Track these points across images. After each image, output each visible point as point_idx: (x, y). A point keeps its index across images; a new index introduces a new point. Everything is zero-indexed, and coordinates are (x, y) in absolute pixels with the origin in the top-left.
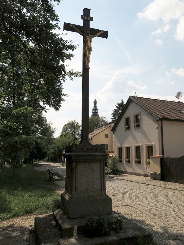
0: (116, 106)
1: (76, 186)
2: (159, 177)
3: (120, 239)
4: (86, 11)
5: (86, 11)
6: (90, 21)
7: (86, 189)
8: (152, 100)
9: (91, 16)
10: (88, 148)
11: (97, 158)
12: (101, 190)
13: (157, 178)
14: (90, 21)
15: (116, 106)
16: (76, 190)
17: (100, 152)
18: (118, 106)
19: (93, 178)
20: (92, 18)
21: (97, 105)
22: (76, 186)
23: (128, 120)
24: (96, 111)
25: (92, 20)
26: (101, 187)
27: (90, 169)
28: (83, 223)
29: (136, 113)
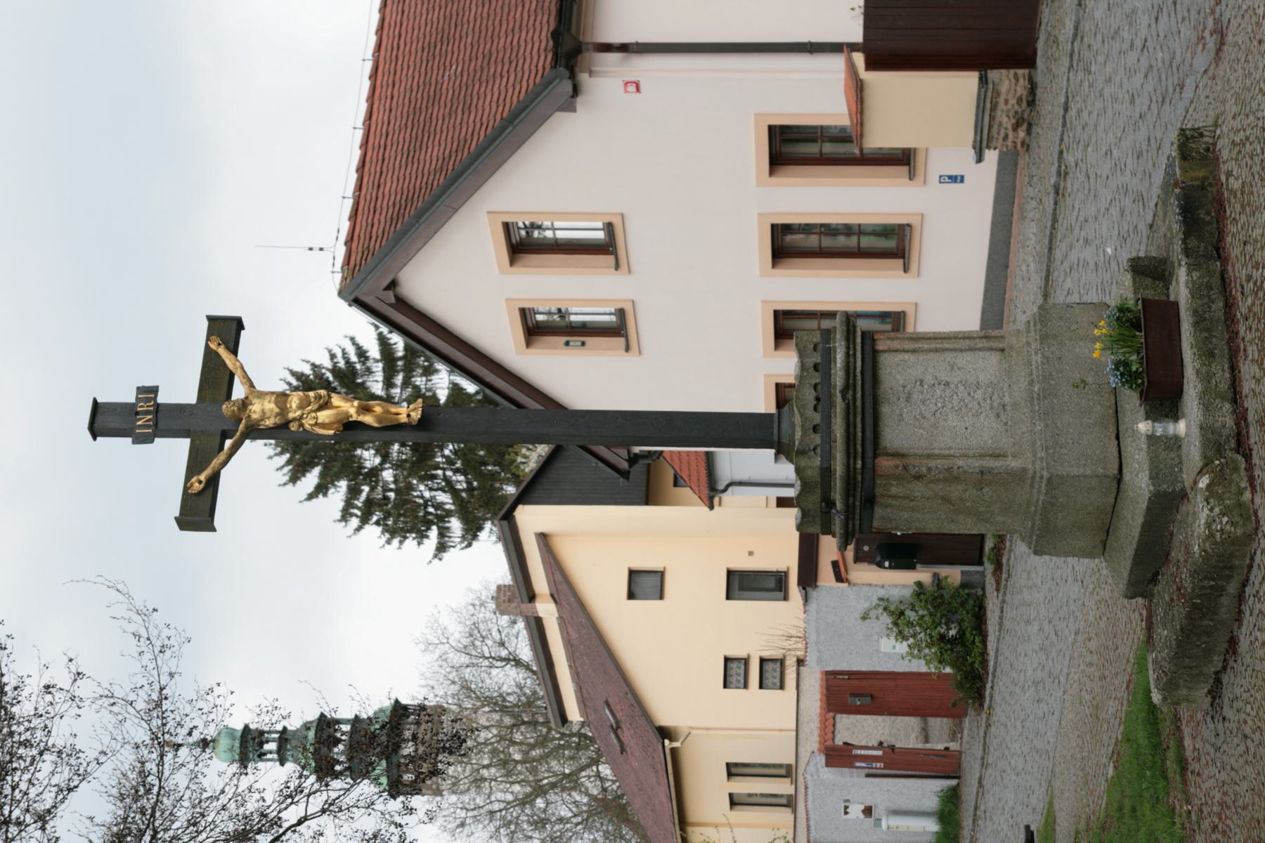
0: (311, 497)
1: (982, 456)
2: (1007, 82)
3: (1187, 256)
6: (160, 400)
7: (998, 416)
8: (379, 116)
9: (130, 398)
11: (859, 363)
12: (1002, 350)
13: (1019, 100)
14: (160, 400)
15: (311, 497)
16: (999, 456)
17: (828, 355)
18: (312, 478)
19: (947, 384)
20: (141, 390)
22: (982, 456)
25: (154, 390)
26: (991, 349)
27: (908, 399)
28: (1131, 400)
29: (494, 248)
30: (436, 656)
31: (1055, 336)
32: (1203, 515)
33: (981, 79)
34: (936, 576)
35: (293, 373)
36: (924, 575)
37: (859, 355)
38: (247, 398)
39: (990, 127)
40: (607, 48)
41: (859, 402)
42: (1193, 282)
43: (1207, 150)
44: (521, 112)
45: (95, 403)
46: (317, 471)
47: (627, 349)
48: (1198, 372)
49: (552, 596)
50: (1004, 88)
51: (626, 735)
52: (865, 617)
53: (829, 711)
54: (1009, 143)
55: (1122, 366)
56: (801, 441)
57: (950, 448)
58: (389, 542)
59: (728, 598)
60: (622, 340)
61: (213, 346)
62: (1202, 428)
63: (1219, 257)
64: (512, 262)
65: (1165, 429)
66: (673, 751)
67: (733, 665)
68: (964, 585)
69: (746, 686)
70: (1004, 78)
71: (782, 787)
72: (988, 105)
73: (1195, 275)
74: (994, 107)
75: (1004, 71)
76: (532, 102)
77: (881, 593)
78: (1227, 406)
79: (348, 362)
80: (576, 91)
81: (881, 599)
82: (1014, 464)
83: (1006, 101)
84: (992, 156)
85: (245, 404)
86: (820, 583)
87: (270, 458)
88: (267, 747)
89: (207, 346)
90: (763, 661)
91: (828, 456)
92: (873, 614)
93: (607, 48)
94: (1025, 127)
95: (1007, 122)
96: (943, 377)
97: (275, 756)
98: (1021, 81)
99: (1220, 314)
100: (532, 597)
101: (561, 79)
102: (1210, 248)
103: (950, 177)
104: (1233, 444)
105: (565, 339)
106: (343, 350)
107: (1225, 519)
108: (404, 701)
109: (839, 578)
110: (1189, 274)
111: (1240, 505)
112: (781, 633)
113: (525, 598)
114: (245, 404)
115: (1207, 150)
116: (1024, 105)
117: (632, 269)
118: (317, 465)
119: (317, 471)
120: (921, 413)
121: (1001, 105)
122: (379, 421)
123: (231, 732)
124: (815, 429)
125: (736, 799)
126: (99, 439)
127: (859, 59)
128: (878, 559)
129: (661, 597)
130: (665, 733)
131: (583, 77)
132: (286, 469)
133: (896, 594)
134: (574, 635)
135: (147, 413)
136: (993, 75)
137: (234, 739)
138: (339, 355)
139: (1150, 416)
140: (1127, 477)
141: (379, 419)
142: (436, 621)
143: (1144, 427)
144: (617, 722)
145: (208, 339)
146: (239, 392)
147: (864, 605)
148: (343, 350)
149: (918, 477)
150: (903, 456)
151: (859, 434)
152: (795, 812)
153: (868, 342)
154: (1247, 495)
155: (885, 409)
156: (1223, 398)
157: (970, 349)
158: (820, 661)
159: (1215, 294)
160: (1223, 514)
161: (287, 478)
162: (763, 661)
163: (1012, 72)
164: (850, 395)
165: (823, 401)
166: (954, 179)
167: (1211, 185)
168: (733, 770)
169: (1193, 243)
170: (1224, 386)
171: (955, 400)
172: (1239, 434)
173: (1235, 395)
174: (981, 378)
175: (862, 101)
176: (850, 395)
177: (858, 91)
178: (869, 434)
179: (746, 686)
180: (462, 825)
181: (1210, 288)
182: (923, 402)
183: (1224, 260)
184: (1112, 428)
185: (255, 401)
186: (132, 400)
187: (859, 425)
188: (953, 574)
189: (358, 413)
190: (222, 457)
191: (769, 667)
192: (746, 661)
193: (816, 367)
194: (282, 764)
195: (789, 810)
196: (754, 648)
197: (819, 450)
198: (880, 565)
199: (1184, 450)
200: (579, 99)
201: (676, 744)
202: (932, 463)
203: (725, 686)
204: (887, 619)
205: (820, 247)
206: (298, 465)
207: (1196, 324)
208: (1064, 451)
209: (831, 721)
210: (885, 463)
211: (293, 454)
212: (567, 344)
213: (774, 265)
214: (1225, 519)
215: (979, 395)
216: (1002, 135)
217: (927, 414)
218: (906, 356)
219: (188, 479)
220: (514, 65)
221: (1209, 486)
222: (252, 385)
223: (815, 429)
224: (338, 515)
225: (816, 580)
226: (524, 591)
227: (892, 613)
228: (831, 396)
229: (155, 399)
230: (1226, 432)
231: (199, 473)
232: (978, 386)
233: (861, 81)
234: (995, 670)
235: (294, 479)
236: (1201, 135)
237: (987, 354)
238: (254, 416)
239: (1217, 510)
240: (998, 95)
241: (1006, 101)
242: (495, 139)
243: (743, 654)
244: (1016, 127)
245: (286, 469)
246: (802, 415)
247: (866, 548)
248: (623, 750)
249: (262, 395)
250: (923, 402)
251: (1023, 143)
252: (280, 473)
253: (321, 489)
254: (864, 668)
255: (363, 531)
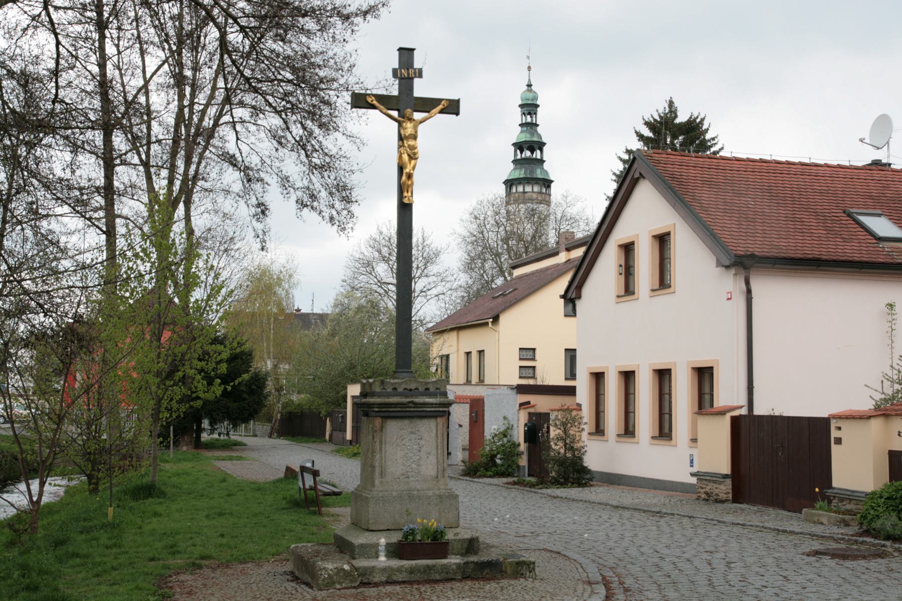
2: (725, 489)
3: (464, 563)
4: (406, 54)
5: (406, 54)
7: (403, 475)
9: (417, 65)
10: (409, 388)
11: (429, 409)
12: (437, 477)
13: (717, 495)
17: (434, 395)
18: (647, 133)
19: (420, 451)
20: (420, 71)
21: (542, 116)
23: (628, 249)
24: (537, 154)
25: (420, 75)
26: (438, 472)
27: (412, 433)
28: (396, 537)
30: (560, 201)
31: (441, 502)
32: (330, 566)
33: (727, 475)
34: (523, 453)
35: (703, 120)
36: (523, 447)
37: (433, 409)
38: (414, 120)
39: (706, 480)
40: (747, 283)
41: (408, 409)
42: (450, 566)
43: (522, 574)
44: (715, 239)
45: (413, 50)
46: (651, 135)
47: (618, 297)
48: (402, 566)
49: (569, 260)
50: (722, 487)
51: (500, 300)
52: (505, 418)
53: (471, 400)
54: (700, 490)
55: (412, 532)
56: (389, 382)
57: (385, 452)
58: (614, 174)
59: (566, 350)
60: (623, 294)
61: (443, 102)
62: (373, 567)
63: (464, 578)
64: (654, 237)
65: (381, 551)
66: (487, 324)
67: (531, 353)
68: (518, 467)
69: (521, 359)
70: (727, 487)
71: (475, 379)
72: (714, 479)
73: (454, 567)
74: (715, 482)
75: (730, 487)
76: (720, 244)
77: (515, 426)
78: (384, 579)
79: (711, 147)
80: (727, 267)
81: (512, 426)
82: (377, 482)
83: (717, 488)
84: (694, 480)
85: (411, 119)
86: (519, 395)
87: (657, 111)
88: (529, 117)
89: (443, 100)
90: (534, 368)
91: (380, 395)
92: (506, 422)
93: (747, 283)
94: (707, 498)
95: (708, 489)
96: (423, 449)
97: (524, 122)
98: (725, 496)
99: (433, 577)
100: (568, 250)
101: (729, 259)
102: (468, 574)
103: (692, 460)
104: (365, 581)
105: (623, 264)
106: (716, 143)
107: (326, 576)
108: (553, 185)
109: (521, 405)
110: (455, 564)
111: (334, 583)
112: (545, 376)
113: (568, 246)
114: (411, 119)
115: (522, 574)
116: (715, 497)
117: (653, 298)
118: (654, 134)
119: (651, 135)
120: (404, 439)
121: (716, 486)
122: (404, 183)
123: (536, 98)
124: (395, 389)
125: (482, 354)
126: (398, 52)
127: (744, 411)
128: (529, 424)
129: (566, 316)
130: (496, 319)
131: (733, 271)
132: (652, 120)
133: (515, 433)
134: (551, 271)
135: (408, 74)
136: (729, 482)
137: (532, 100)
138: (714, 142)
139: (388, 545)
140: (367, 534)
141: (404, 183)
142: (578, 201)
143: (383, 541)
144: (506, 295)
145: (447, 100)
146: (418, 116)
147: (510, 417)
148: (716, 143)
149: (373, 437)
150: (382, 430)
151: (391, 410)
152: (464, 384)
153: (441, 413)
154: (338, 586)
155: (407, 422)
156: (388, 577)
157: (438, 462)
158: (488, 396)
159: (444, 576)
160: (329, 575)
161: (647, 120)
162: (534, 368)
163: (731, 491)
164: (411, 405)
165: (409, 392)
166: (692, 462)
167: (502, 575)
168: (481, 352)
169: (472, 566)
170: (395, 578)
171: (411, 455)
172: (370, 584)
173: (389, 582)
174: (423, 467)
175: (716, 414)
176: (411, 405)
177: (722, 413)
178: (392, 414)
179: (521, 359)
180: (476, 218)
181: (447, 573)
182: (410, 440)
183: (460, 581)
184: (393, 527)
185: (412, 124)
186: (415, 66)
187: (396, 409)
188: (523, 462)
189: (406, 173)
190: (385, 110)
191: (531, 371)
192: (533, 359)
193: (427, 389)
194: (520, 125)
195: (465, 381)
196: (540, 363)
197: (384, 391)
198: (526, 425)
199: (374, 560)
200: (724, 269)
201: (490, 324)
202: (377, 444)
203: (520, 349)
204: (502, 429)
205: (704, 394)
206: (653, 125)
207: (428, 566)
208: (381, 505)
209: (465, 401)
210: (378, 421)
211: (661, 123)
212: (621, 266)
213: (655, 371)
214: (326, 576)
215: (414, 466)
216: (703, 486)
217: (403, 442)
218: (434, 432)
219: (374, 95)
220: (744, 234)
221: (344, 569)
222: (421, 122)
223: (395, 389)
224: (629, 148)
225: (520, 393)
226: (571, 245)
227: (505, 431)
228: (412, 396)
229: (416, 77)
230: (371, 578)
231: (376, 100)
232: (419, 465)
233: (725, 414)
234: (473, 482)
235: (647, 124)
236: (530, 572)
237: (435, 470)
238: (404, 124)
239: (331, 572)
240: (719, 484)
241: (717, 488)
242: (704, 226)
243: (537, 357)
244: (706, 493)
245: (652, 120)
246: (403, 382)
247: (534, 418)
248: (494, 298)
249: (415, 128)
250: (410, 440)
251: (699, 497)
252: (650, 116)
253: (641, 137)
254: (485, 418)
255: (619, 161)
